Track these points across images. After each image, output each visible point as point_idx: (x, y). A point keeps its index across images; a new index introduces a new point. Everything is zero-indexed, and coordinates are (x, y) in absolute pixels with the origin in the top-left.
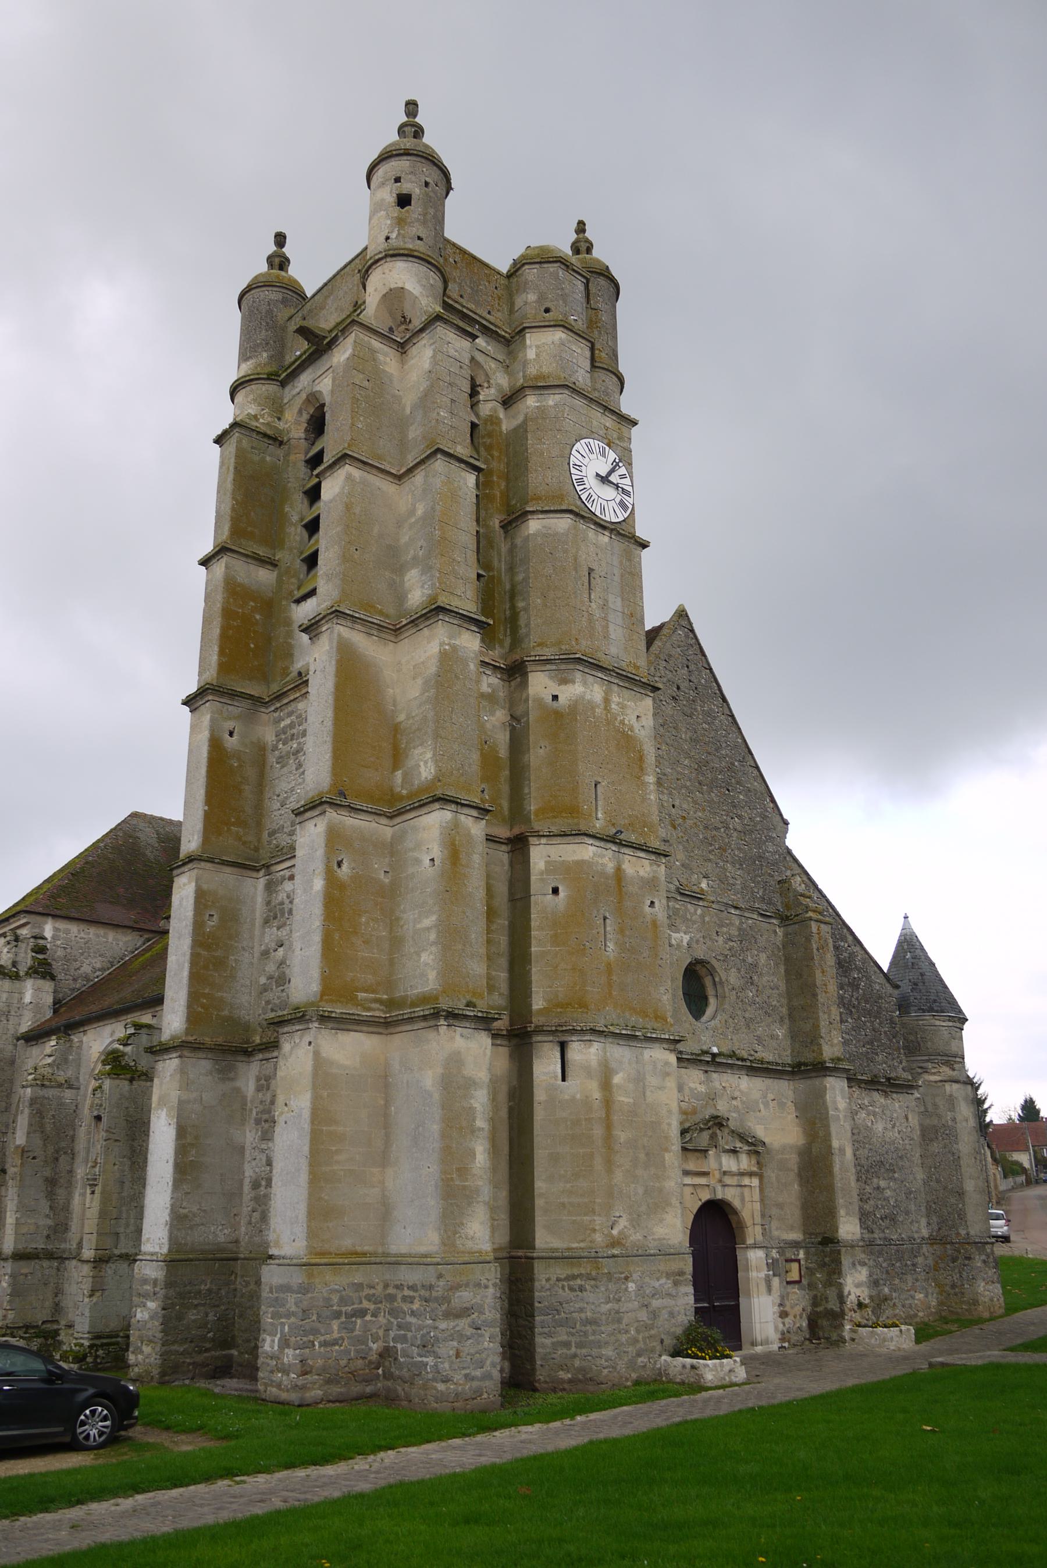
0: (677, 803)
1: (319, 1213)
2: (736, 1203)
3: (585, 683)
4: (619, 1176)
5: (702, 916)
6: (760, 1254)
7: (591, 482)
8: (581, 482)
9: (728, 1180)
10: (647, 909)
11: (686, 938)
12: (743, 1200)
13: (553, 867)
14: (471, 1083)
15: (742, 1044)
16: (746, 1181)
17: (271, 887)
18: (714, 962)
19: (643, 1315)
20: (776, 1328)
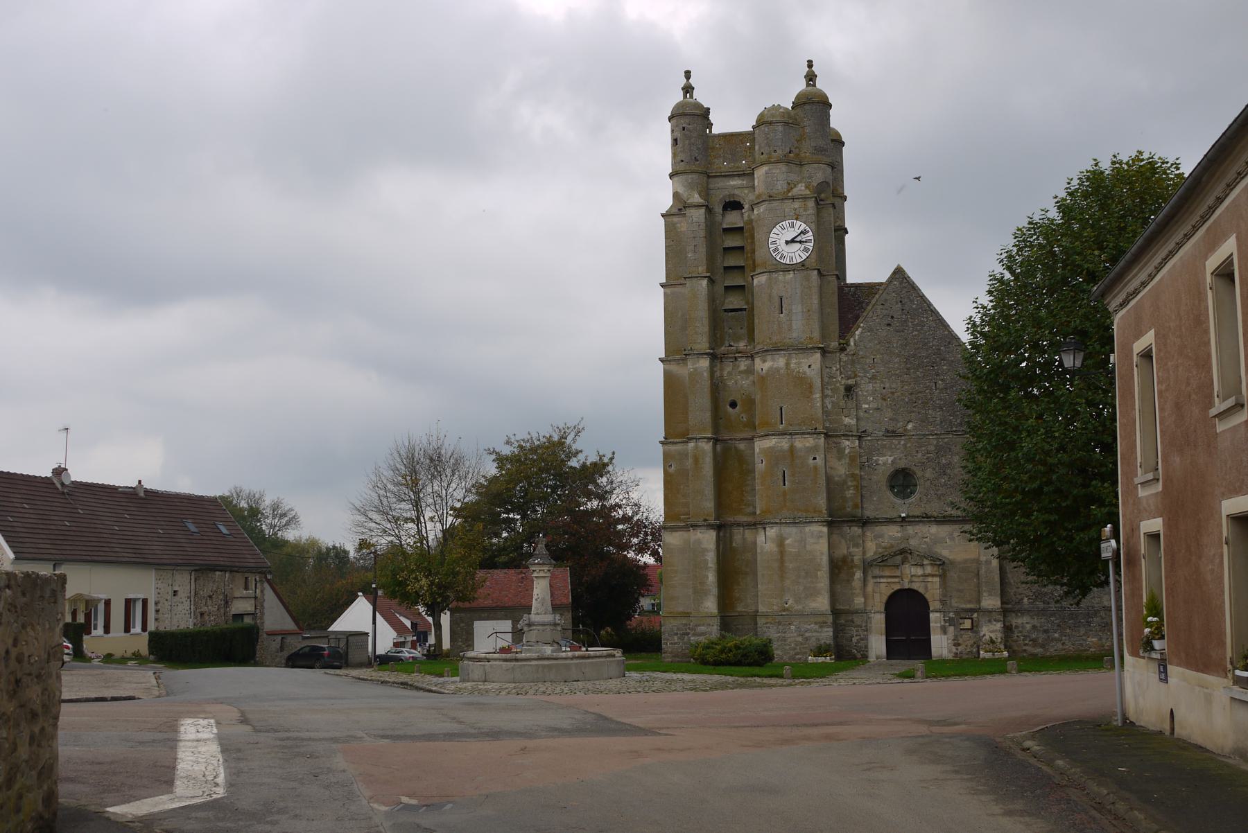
0: (887, 385)
1: (970, 602)
2: (921, 590)
3: (773, 360)
4: (788, 583)
5: (905, 445)
6: (938, 615)
7: (783, 247)
8: (776, 250)
9: (914, 579)
10: (811, 461)
11: (890, 459)
12: (926, 588)
13: (764, 451)
14: (705, 550)
15: (934, 508)
16: (930, 579)
17: (137, 656)
18: (914, 468)
19: (800, 639)
20: (950, 651)
